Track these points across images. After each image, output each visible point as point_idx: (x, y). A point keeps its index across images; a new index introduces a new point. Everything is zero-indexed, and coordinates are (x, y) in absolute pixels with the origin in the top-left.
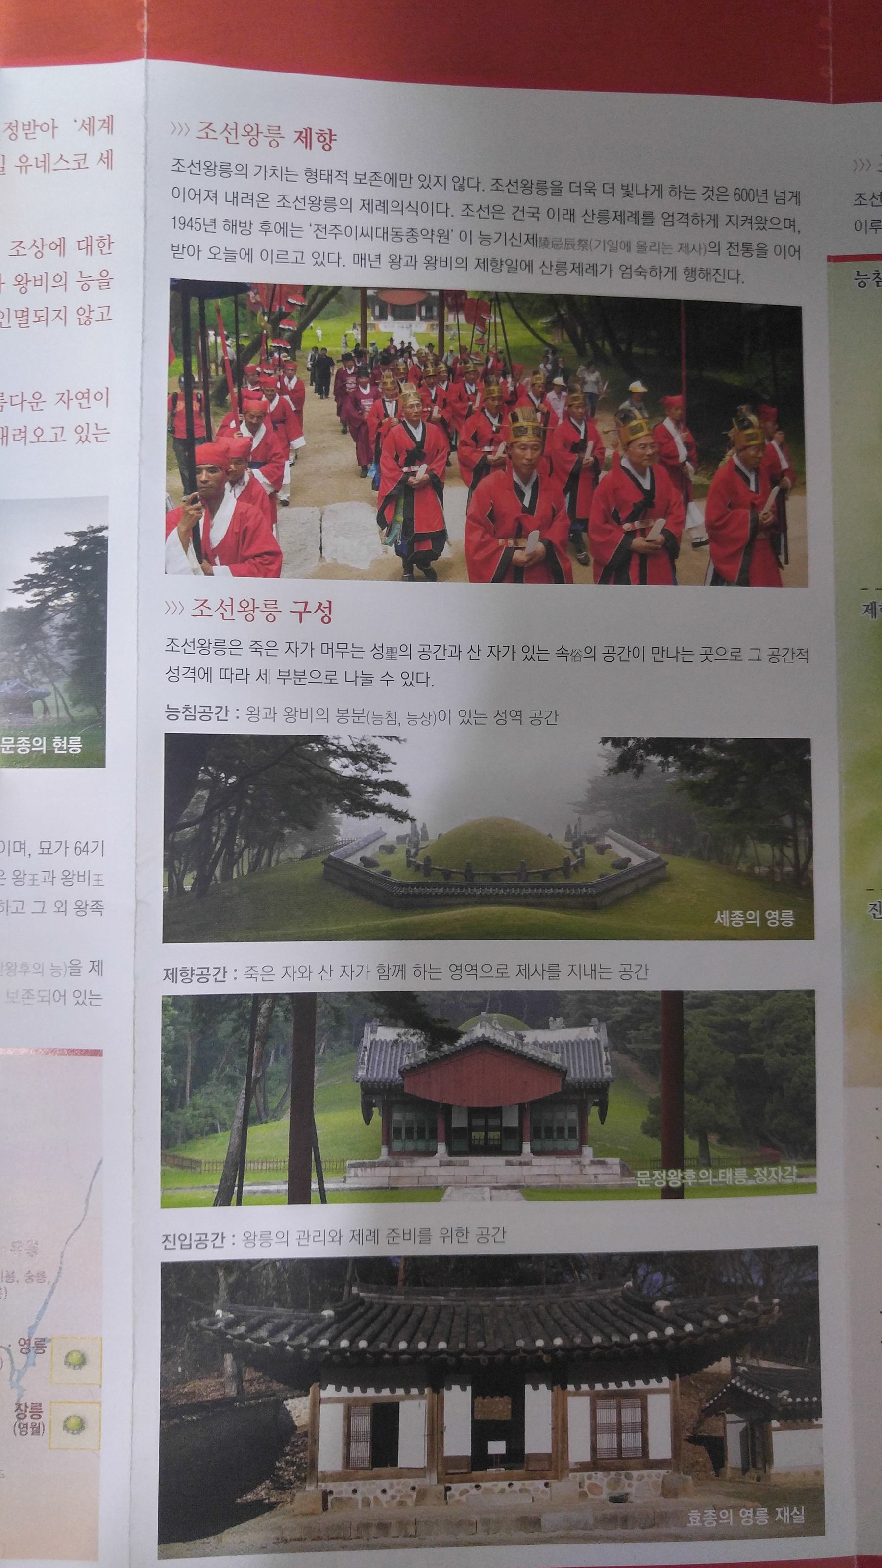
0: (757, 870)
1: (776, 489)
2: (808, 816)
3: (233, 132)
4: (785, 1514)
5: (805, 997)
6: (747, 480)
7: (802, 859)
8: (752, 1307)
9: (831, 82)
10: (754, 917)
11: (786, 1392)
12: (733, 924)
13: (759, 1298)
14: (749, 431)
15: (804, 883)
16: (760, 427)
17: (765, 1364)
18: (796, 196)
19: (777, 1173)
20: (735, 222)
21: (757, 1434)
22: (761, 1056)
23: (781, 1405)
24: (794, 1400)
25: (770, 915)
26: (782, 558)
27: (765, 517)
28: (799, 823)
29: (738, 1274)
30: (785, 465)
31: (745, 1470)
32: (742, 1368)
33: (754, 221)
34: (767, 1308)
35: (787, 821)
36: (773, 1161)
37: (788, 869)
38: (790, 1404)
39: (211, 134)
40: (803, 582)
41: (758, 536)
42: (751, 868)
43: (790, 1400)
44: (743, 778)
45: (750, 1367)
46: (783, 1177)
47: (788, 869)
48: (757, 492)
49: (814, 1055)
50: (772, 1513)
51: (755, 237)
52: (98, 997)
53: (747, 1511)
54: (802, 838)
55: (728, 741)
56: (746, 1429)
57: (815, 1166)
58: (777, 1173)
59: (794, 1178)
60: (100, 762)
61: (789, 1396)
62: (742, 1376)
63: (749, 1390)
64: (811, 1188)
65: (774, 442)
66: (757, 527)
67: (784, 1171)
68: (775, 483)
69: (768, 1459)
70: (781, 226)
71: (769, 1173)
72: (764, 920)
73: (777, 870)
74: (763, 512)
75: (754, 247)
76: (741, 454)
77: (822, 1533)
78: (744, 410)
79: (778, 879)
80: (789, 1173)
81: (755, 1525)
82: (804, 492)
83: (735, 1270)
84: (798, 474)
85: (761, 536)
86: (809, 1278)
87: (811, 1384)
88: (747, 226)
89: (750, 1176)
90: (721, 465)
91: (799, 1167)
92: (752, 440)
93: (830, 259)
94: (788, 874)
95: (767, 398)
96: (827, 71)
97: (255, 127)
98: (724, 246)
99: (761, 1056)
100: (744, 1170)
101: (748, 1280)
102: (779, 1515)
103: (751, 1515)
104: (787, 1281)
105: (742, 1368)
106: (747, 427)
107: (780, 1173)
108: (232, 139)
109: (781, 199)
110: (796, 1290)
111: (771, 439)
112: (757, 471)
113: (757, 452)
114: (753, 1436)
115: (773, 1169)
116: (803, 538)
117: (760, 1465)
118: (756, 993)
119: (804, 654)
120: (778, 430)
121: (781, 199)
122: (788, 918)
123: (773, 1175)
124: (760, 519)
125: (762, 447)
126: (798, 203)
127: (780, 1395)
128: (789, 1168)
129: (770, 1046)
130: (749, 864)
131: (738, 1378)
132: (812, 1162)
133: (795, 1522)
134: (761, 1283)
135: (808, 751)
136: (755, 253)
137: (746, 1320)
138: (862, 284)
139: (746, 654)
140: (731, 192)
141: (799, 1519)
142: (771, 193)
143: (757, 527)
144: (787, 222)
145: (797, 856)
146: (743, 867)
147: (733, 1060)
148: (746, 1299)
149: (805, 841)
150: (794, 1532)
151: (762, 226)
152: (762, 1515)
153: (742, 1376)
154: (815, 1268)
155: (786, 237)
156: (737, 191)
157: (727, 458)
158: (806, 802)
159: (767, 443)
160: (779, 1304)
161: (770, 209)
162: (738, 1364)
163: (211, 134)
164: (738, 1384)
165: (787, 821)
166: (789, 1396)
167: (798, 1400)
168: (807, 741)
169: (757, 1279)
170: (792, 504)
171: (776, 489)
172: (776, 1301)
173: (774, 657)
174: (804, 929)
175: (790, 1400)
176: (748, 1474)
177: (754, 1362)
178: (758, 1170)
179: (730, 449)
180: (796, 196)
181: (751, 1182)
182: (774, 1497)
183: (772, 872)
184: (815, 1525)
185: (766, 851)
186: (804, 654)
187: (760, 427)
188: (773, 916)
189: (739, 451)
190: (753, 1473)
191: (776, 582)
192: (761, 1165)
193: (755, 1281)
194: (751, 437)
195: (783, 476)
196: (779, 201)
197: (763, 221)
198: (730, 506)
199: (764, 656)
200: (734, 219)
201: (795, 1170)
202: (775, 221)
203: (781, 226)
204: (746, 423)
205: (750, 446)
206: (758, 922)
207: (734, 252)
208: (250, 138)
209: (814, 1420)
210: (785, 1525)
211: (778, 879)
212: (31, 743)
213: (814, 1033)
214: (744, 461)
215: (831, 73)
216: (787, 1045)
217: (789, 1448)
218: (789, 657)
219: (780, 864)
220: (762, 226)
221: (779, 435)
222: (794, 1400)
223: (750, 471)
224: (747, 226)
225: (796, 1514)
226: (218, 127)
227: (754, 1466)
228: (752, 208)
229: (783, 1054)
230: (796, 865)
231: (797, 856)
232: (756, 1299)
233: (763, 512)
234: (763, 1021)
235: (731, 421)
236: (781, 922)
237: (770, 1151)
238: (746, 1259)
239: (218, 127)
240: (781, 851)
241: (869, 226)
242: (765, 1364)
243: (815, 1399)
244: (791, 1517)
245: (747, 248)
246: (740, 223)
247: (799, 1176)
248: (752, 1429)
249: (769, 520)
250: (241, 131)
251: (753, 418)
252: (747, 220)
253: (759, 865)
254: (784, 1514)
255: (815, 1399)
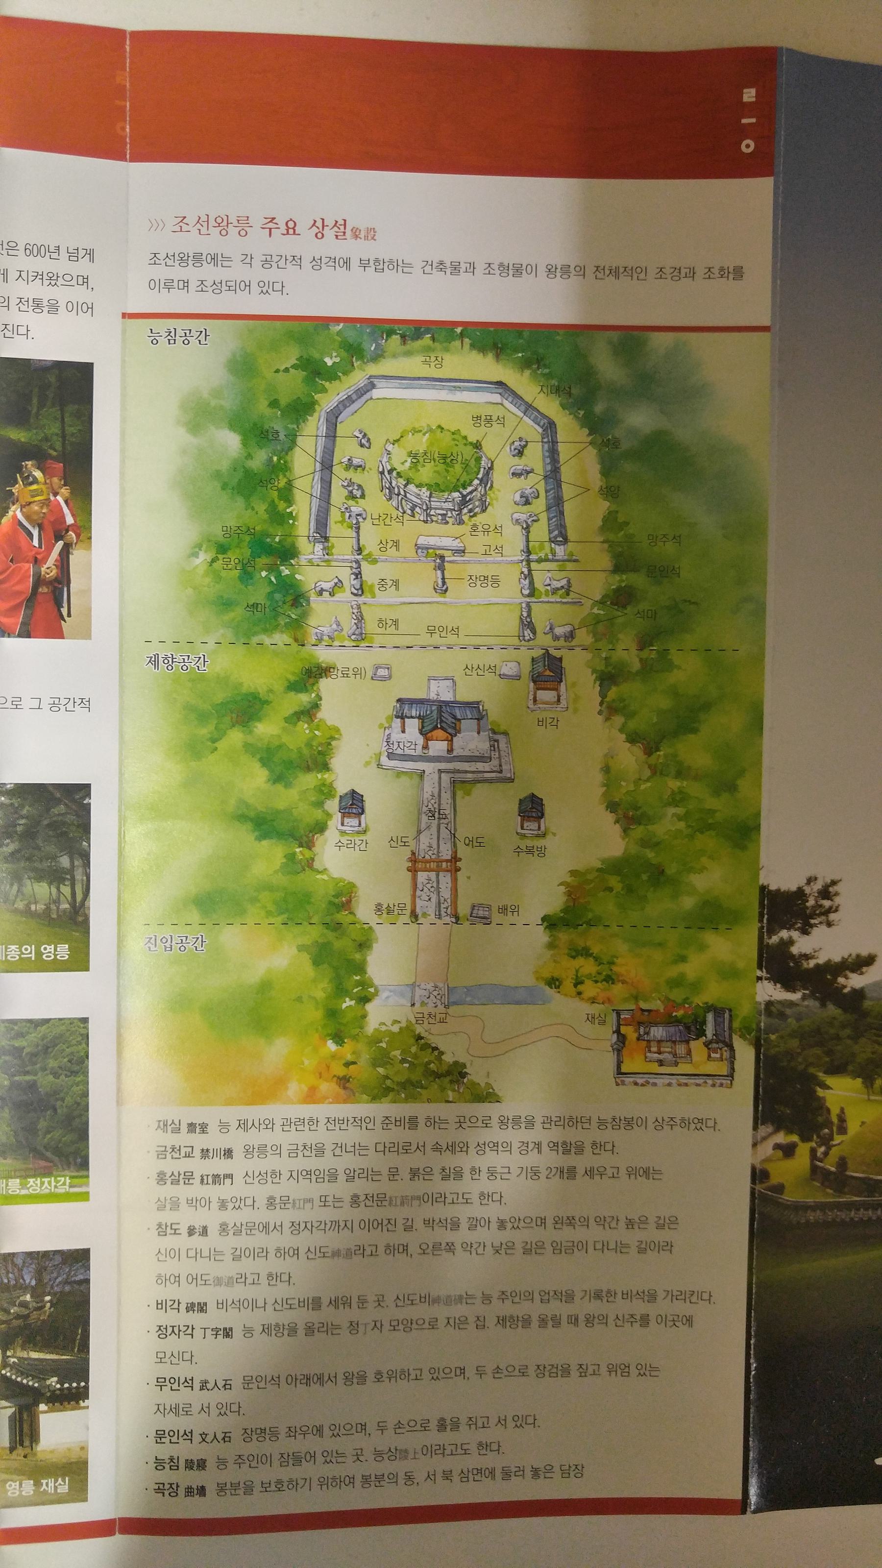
0: (33, 907)
1: (60, 544)
2: (86, 857)
3: (205, 224)
4: (50, 1485)
5: (79, 1023)
6: (30, 535)
7: (79, 897)
8: (24, 1305)
9: (128, 140)
10: (29, 951)
11: (55, 1379)
12: (9, 957)
13: (32, 1297)
14: (34, 487)
15: (80, 919)
16: (46, 483)
17: (34, 1355)
18: (90, 253)
19: (50, 1183)
20: (26, 279)
21: (25, 1416)
22: (34, 1078)
23: (49, 1391)
24: (62, 1385)
25: (45, 949)
26: (64, 611)
27: (48, 571)
28: (76, 863)
29: (11, 1275)
30: (70, 520)
31: (12, 1449)
32: (12, 1360)
33: (45, 277)
34: (39, 1305)
35: (65, 861)
36: (47, 1172)
37: (65, 906)
38: (59, 1389)
39: (185, 228)
40: (86, 635)
41: (40, 590)
42: (28, 906)
43: (58, 1386)
44: (23, 821)
45: (19, 1358)
46: (56, 1187)
47: (65, 906)
48: (40, 547)
49: (87, 1077)
50: (37, 1484)
51: (45, 292)
52: (657, 1369)
53: (13, 1484)
54: (79, 875)
55: (8, 786)
56: (14, 1413)
57: (88, 1176)
58: (50, 1183)
59: (67, 1187)
60: (84, 966)
61: (57, 1383)
62: (13, 1367)
63: (19, 1379)
64: (84, 1197)
65: (58, 498)
66: (39, 581)
67: (57, 1182)
68: (58, 537)
69: (34, 1437)
70: (74, 282)
71: (42, 1183)
72: (39, 954)
73: (53, 907)
74: (46, 566)
75: (45, 303)
76: (24, 510)
77: (85, 1500)
78: (29, 466)
79: (54, 916)
80: (62, 1182)
81: (20, 1495)
82: (89, 547)
83: (8, 1272)
84: (83, 530)
85: (43, 590)
86: (81, 1277)
87: (82, 1371)
88: (38, 281)
89: (23, 1186)
90: (4, 520)
91: (71, 1177)
92: (38, 495)
93: (124, 315)
94: (65, 911)
95: (55, 454)
96: (124, 129)
97: (225, 218)
98: (14, 301)
99: (34, 1078)
100: (18, 1180)
101: (21, 1281)
102: (44, 1486)
103: (18, 1487)
104: (60, 1279)
105: (12, 1360)
106: (31, 484)
107: (53, 1184)
108: (204, 230)
109: (74, 256)
110: (67, 1288)
111: (56, 494)
112: (41, 527)
113: (42, 508)
114: (21, 1419)
115: (46, 1180)
116: (87, 592)
117: (27, 1443)
118: (30, 1021)
119: (85, 703)
120: (65, 485)
121: (74, 256)
122: (63, 951)
123: (46, 1184)
124: (43, 573)
125: (46, 503)
126: (92, 260)
127: (48, 1382)
128: (63, 1179)
129: (44, 1069)
130: (26, 902)
131: (8, 1369)
132: (85, 1173)
133: (59, 1491)
134: (33, 1283)
135: (89, 795)
136: (46, 309)
137: (18, 1317)
138: (155, 342)
139: (27, 703)
140: (21, 247)
141: (64, 1489)
142: (63, 250)
143: (39, 581)
144: (80, 279)
145: (74, 894)
146: (20, 905)
147: (6, 1083)
148: (19, 1297)
149: (83, 880)
150: (60, 1500)
151: (53, 282)
152: (28, 1487)
153: (13, 1367)
154: (88, 1268)
155: (79, 294)
156: (28, 246)
157: (11, 513)
158: (84, 843)
159: (52, 498)
160: (50, 1301)
161: (62, 266)
162: (9, 1357)
163: (185, 228)
164: (8, 1374)
165: (65, 861)
166: (57, 1383)
167: (66, 1385)
168: (87, 787)
169: (29, 1279)
170: (76, 558)
171: (60, 544)
172: (48, 1298)
173: (55, 705)
174: (79, 961)
175: (58, 1386)
176: (15, 1452)
177: (24, 1354)
178: (31, 1180)
179: (14, 504)
180: (90, 253)
181: (24, 1192)
182: (40, 1471)
183: (48, 908)
184: (79, 1492)
185: (43, 890)
186: (85, 703)
187: (46, 483)
188: (48, 950)
189: (22, 507)
190: (20, 1451)
191: (57, 633)
192: (34, 1176)
193: (27, 1282)
194: (35, 494)
195: (67, 531)
196: (71, 258)
197: (55, 278)
198: (12, 561)
199: (45, 705)
200: (24, 275)
201: (68, 1181)
202: (68, 278)
203: (74, 282)
204: (31, 479)
205: (34, 502)
206: (33, 955)
207: (23, 308)
208: (220, 228)
209: (81, 1402)
210: (51, 1494)
211: (54, 916)
212: (21, 951)
213: (87, 1057)
214: (28, 518)
215: (128, 130)
216: (60, 1067)
217: (56, 1429)
218: (70, 706)
219: (57, 902)
220: (53, 282)
221: (65, 491)
222: (62, 1385)
223: (34, 527)
224: (38, 281)
225: (60, 1484)
226: (191, 220)
227: (22, 1445)
228: (43, 264)
229: (56, 1075)
230: (73, 903)
231: (74, 894)
232: (28, 1298)
233: (46, 566)
234: (38, 1046)
235: (16, 478)
236: (55, 955)
237: (43, 1163)
238: (19, 1261)
239: (191, 220)
240: (58, 889)
241: (162, 285)
242: (34, 1355)
243: (83, 1384)
244: (56, 1488)
245: (37, 304)
246: (31, 278)
247: (71, 1186)
248: (21, 1413)
249: (51, 574)
250: (212, 222)
251: (38, 474)
252: (38, 275)
253: (36, 903)
254: (49, 1485)
255: (83, 1384)
